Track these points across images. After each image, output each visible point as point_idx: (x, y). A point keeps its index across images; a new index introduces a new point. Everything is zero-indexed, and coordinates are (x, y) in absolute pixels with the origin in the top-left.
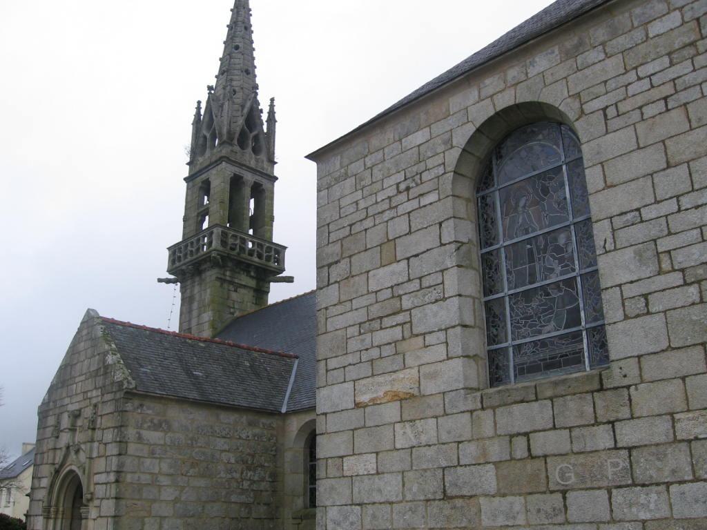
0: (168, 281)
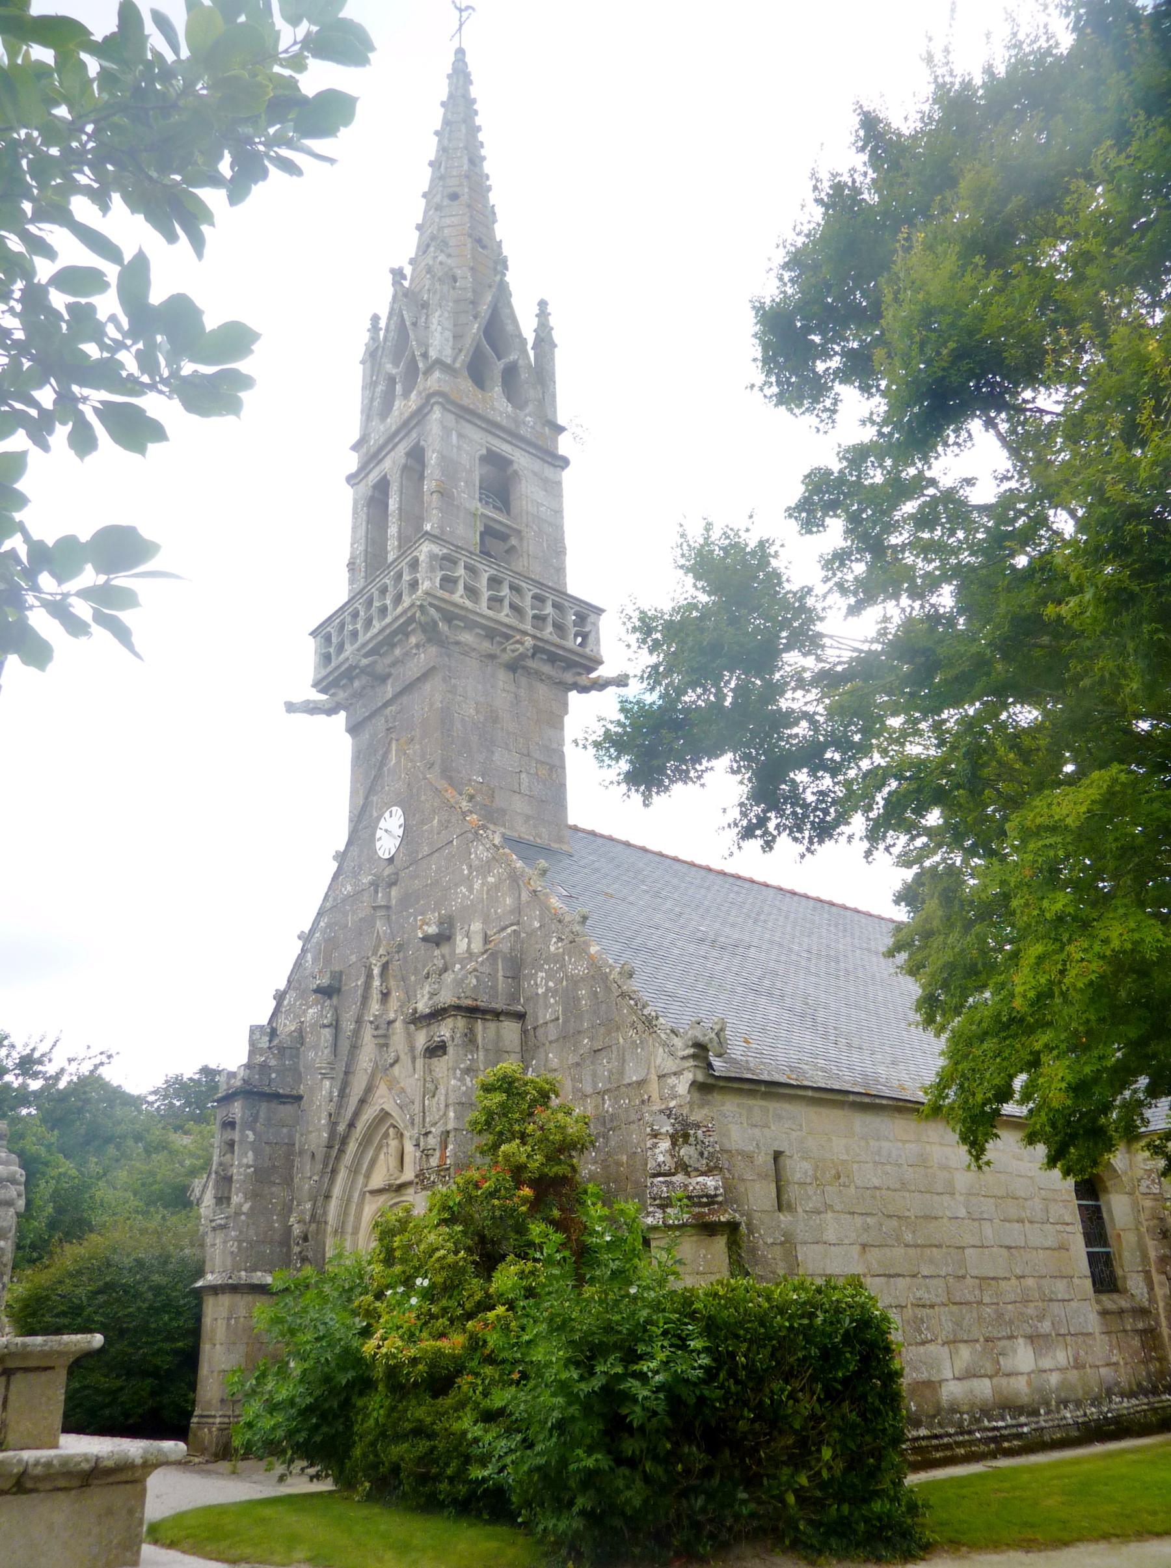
0: (312, 709)
